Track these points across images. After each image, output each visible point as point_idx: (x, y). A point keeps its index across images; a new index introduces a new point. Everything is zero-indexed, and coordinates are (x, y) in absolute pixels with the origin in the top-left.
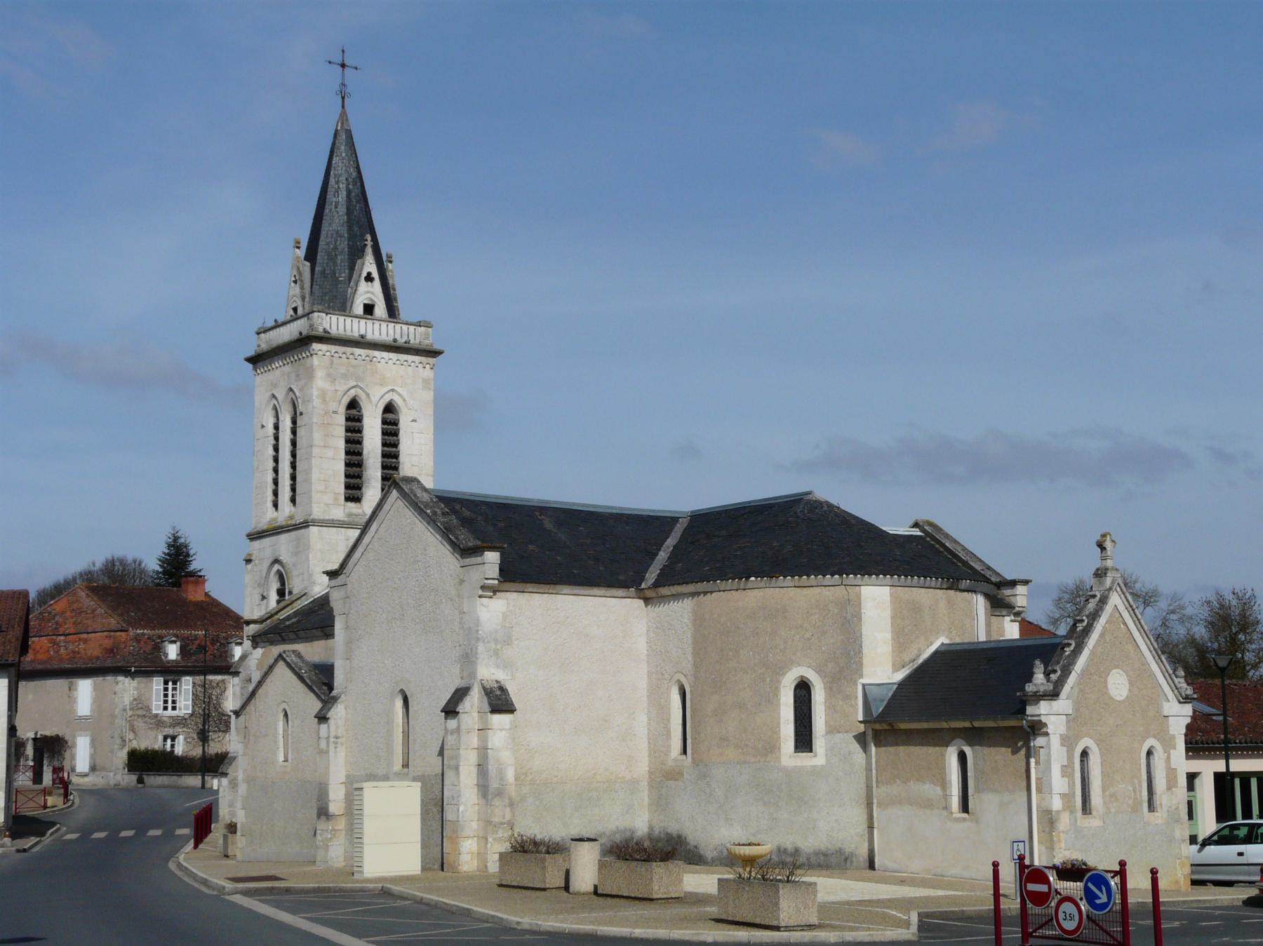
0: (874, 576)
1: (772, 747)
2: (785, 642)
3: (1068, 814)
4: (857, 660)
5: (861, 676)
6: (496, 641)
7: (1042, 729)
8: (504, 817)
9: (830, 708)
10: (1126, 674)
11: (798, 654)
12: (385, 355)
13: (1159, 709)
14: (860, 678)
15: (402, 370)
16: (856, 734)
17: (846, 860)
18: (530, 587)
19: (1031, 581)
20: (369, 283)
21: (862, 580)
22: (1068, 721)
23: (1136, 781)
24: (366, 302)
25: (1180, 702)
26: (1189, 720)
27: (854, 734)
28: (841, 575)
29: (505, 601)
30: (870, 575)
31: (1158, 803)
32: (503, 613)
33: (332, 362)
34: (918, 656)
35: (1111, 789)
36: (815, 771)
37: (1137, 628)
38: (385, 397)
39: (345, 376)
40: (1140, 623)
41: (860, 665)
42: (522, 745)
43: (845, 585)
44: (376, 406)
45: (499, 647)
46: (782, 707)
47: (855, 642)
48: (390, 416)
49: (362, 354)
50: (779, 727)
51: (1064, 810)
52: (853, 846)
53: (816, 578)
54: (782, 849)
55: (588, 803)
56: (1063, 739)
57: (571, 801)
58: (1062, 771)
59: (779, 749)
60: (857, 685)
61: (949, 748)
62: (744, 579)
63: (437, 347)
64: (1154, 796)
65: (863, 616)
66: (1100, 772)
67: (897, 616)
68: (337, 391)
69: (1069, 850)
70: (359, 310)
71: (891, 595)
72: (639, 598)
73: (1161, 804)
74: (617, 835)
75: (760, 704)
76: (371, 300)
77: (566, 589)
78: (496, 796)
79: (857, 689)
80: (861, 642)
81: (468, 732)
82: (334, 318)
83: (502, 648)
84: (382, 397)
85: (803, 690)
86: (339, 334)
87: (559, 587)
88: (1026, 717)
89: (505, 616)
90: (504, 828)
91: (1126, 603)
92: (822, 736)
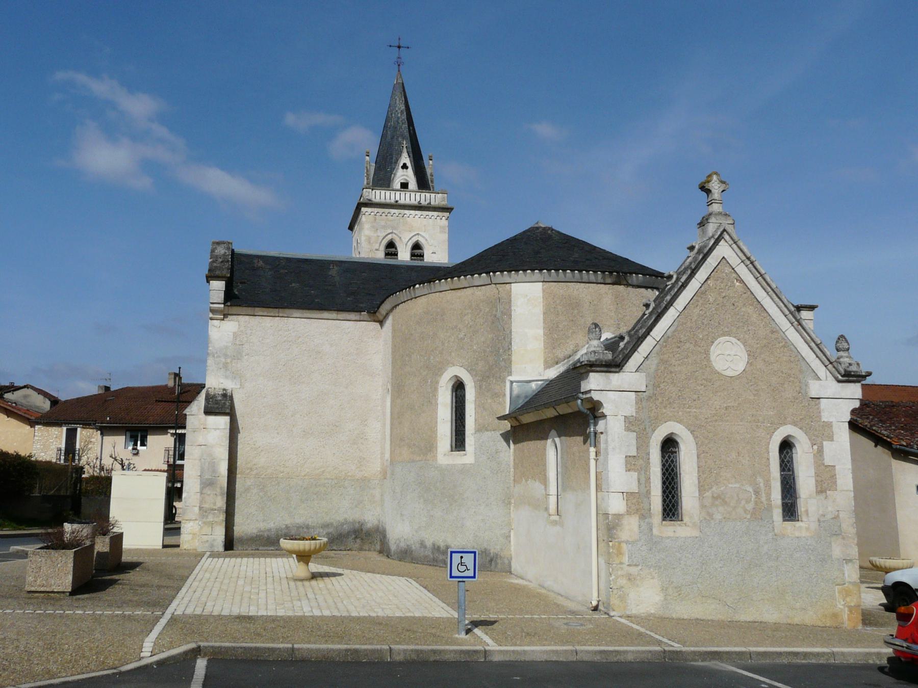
0: (521, 272)
1: (430, 447)
2: (443, 344)
3: (638, 518)
4: (506, 357)
5: (510, 374)
6: (226, 356)
7: (600, 409)
8: (215, 504)
9: (479, 406)
10: (744, 344)
11: (453, 354)
12: (413, 212)
13: (802, 391)
14: (508, 376)
15: (425, 222)
16: (503, 432)
17: (491, 560)
18: (258, 311)
19: (816, 307)
20: (405, 170)
21: (510, 277)
22: (639, 401)
23: (760, 480)
24: (402, 181)
25: (839, 381)
26: (857, 404)
27: (501, 432)
28: (488, 273)
29: (237, 323)
30: (517, 271)
31: (803, 509)
32: (234, 333)
33: (375, 220)
34: (576, 352)
35: (714, 489)
36: (465, 470)
37: (762, 287)
38: (412, 239)
39: (384, 227)
40: (764, 279)
41: (509, 361)
42: (248, 444)
43: (495, 284)
44: (406, 245)
45: (229, 360)
46: (439, 406)
47: (504, 339)
48: (417, 252)
49: (396, 213)
50: (436, 426)
51: (629, 513)
52: (498, 547)
53: (466, 279)
54: (436, 547)
55: (315, 496)
56: (630, 422)
57: (297, 493)
58: (627, 463)
59: (436, 448)
60: (505, 382)
61: (548, 440)
62: (412, 288)
63: (449, 206)
64: (798, 500)
65: (513, 313)
66: (695, 466)
67: (550, 312)
68: (378, 236)
69: (636, 565)
70: (398, 186)
71: (544, 291)
72: (375, 321)
73: (807, 511)
74: (345, 526)
75: (423, 405)
76: (406, 180)
77: (297, 313)
78: (207, 486)
79: (505, 386)
80: (511, 339)
81: (194, 431)
82: (378, 192)
83: (231, 362)
84: (410, 239)
85: (459, 388)
86: (386, 202)
87: (288, 311)
88: (581, 395)
89: (235, 335)
90: (214, 514)
91: (741, 254)
92: (472, 434)
